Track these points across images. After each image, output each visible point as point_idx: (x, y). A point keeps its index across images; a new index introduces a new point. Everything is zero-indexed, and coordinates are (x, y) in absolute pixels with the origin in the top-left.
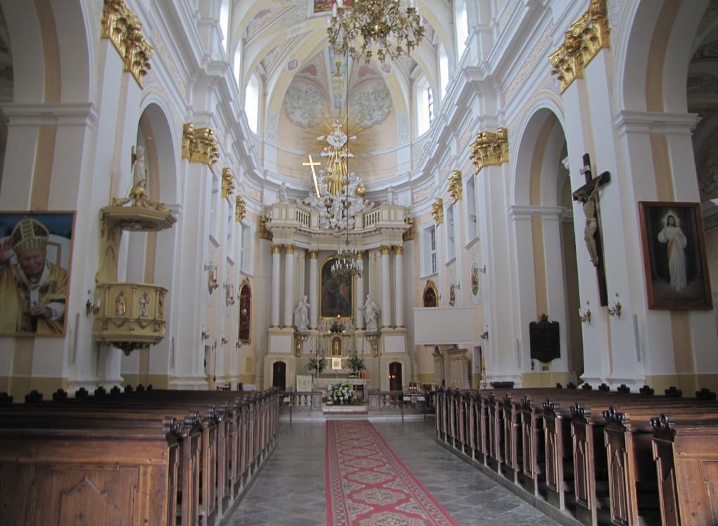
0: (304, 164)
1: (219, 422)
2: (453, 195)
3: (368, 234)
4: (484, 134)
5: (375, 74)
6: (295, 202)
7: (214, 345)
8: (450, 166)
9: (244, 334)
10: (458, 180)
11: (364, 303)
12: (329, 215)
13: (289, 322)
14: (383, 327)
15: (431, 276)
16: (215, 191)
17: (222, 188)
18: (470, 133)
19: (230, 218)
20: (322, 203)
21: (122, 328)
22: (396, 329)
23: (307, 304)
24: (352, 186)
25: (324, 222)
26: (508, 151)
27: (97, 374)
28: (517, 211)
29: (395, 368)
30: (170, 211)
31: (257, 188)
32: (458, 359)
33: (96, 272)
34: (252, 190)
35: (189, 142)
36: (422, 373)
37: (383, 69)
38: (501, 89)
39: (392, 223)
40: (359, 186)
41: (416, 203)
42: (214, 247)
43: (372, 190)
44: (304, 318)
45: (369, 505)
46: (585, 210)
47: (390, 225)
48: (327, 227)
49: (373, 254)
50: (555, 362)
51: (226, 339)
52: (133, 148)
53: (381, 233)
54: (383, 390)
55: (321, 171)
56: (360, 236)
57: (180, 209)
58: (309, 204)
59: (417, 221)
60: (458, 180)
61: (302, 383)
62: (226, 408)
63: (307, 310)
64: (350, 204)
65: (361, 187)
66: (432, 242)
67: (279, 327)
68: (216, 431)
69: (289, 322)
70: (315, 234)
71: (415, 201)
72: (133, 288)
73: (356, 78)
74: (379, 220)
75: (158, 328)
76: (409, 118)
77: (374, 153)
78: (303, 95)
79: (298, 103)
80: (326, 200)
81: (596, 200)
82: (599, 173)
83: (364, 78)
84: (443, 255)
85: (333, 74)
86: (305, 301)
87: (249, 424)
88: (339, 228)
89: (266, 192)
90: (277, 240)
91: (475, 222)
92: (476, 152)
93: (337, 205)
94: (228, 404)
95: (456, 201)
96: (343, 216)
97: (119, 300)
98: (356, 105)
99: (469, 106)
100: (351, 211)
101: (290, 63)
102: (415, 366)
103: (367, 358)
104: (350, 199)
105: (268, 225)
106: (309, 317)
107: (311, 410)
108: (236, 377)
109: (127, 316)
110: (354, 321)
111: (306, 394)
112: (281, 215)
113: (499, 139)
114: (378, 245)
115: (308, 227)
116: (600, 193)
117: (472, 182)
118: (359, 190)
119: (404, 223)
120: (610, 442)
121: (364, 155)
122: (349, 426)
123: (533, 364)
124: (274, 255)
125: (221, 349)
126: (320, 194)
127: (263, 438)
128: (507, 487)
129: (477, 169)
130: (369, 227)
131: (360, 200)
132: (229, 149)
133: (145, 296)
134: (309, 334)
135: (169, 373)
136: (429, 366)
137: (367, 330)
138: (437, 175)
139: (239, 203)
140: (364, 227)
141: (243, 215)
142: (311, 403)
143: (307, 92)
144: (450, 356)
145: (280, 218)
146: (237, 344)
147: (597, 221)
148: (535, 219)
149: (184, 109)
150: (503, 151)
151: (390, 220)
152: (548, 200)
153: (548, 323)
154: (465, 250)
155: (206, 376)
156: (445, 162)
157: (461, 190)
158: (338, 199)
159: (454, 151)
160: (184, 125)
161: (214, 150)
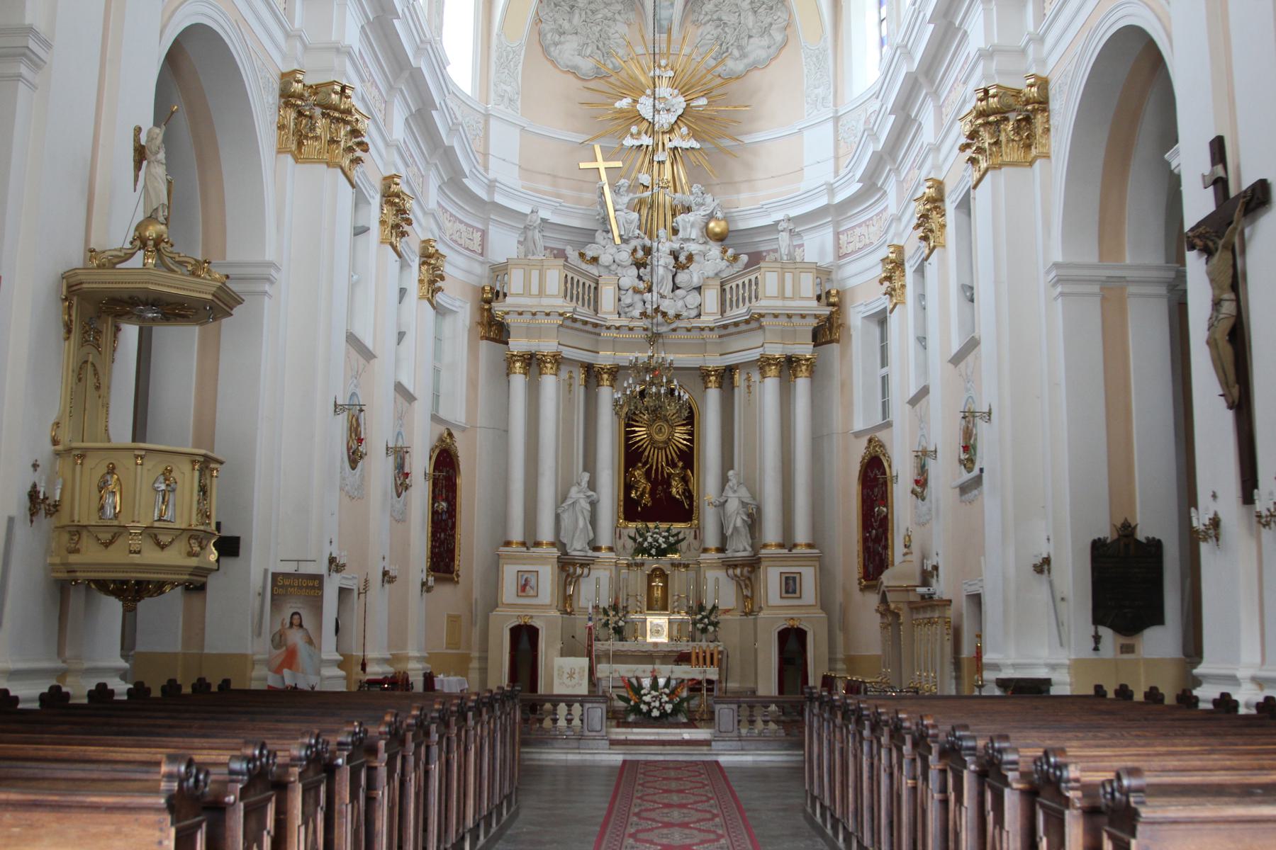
0: (582, 165)
1: (338, 766)
2: (925, 238)
3: (732, 330)
4: (991, 92)
6: (561, 254)
7: (362, 587)
9: (443, 559)
10: (936, 201)
11: (723, 489)
12: (642, 286)
13: (546, 534)
14: (765, 546)
16: (360, 231)
17: (383, 222)
18: (961, 92)
19: (403, 291)
20: (625, 256)
21: (111, 548)
22: (794, 551)
23: (591, 493)
25: (628, 301)
26: (1048, 130)
27: (60, 653)
28: (1064, 276)
29: (792, 642)
30: (227, 277)
31: (476, 224)
32: (930, 622)
33: (53, 418)
34: (462, 227)
35: (294, 115)
40: (711, 216)
41: (846, 255)
42: (362, 361)
43: (742, 225)
46: (1209, 273)
47: (784, 308)
48: (636, 313)
49: (744, 376)
51: (392, 573)
52: (138, 130)
54: (762, 691)
55: (622, 181)
56: (714, 335)
58: (595, 260)
59: (848, 299)
60: (936, 201)
61: (566, 675)
62: (355, 734)
63: (588, 507)
64: (690, 258)
65: (717, 219)
67: (524, 544)
68: (323, 788)
70: (608, 328)
72: (137, 457)
74: (757, 298)
75: (196, 549)
76: (830, 52)
77: (747, 139)
79: (570, 21)
80: (635, 250)
81: (1236, 252)
82: (1248, 181)
84: (904, 384)
87: (427, 772)
88: (664, 314)
90: (518, 345)
91: (972, 300)
92: (973, 135)
93: (662, 261)
94: (361, 724)
96: (676, 287)
97: (106, 482)
99: (961, 23)
103: (728, 617)
104: (693, 247)
105: (498, 308)
106: (593, 521)
107: (581, 738)
108: (419, 659)
109: (123, 521)
110: (698, 534)
111: (569, 700)
113: (1027, 102)
114: (755, 355)
115: (592, 312)
116: (1247, 231)
117: (965, 205)
118: (712, 225)
119: (815, 303)
120: (1047, 833)
121: (726, 143)
122: (672, 774)
124: (512, 377)
125: (379, 597)
126: (621, 236)
127: (471, 802)
129: (977, 175)
130: (736, 312)
131: (715, 250)
132: (398, 130)
133: (167, 474)
137: (729, 553)
138: (891, 188)
139: (429, 257)
142: (582, 720)
144: (915, 616)
146: (424, 584)
147: (1238, 300)
148: (1112, 296)
150: (1039, 130)
151: (784, 298)
152: (1142, 252)
155: (338, 657)
156: (909, 158)
157: (943, 226)
158: (664, 246)
159: (928, 134)
161: (355, 133)
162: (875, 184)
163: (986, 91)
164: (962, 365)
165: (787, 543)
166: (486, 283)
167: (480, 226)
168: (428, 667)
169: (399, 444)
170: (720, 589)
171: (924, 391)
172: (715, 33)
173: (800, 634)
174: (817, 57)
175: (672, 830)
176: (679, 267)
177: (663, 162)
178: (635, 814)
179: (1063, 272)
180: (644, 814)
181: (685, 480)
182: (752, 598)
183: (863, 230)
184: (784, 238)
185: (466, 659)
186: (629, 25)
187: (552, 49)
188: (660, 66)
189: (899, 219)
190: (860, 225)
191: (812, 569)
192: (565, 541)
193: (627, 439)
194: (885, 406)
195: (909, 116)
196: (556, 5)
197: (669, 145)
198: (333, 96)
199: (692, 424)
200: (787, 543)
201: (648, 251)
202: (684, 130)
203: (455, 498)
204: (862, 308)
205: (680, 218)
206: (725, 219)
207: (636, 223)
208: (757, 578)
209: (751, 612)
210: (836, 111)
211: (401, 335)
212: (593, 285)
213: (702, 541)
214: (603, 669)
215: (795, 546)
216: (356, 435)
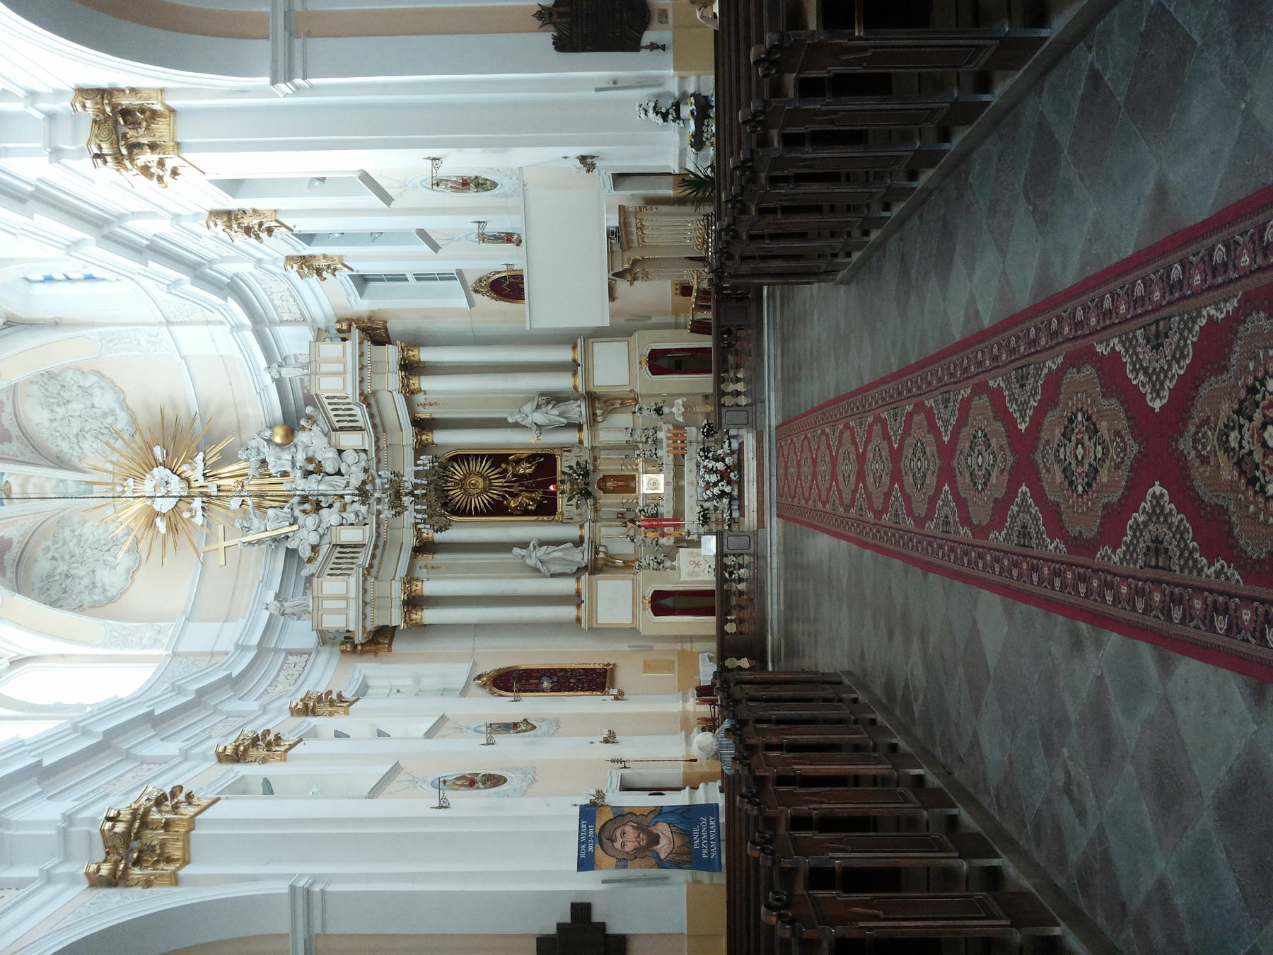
2: (270, 231)
3: (377, 420)
4: (96, 151)
6: (309, 579)
9: (594, 680)
12: (337, 505)
13: (566, 586)
14: (575, 388)
16: (268, 788)
17: (264, 760)
19: (338, 735)
20: (310, 521)
24: (269, 454)
28: (284, 71)
29: (660, 362)
32: (641, 228)
34: (283, 673)
40: (269, 441)
42: (401, 777)
43: (278, 414)
44: (559, 554)
45: (955, 433)
48: (364, 509)
49: (421, 408)
53: (374, 393)
54: (710, 390)
56: (383, 437)
57: (301, 883)
58: (315, 548)
59: (348, 313)
64: (310, 460)
66: (389, 280)
67: (578, 606)
69: (566, 586)
71: (298, 316)
76: (102, 330)
78: (62, 567)
79: (81, 578)
80: (304, 511)
83: (14, 431)
84: (416, 258)
86: (523, 552)
88: (364, 483)
89: (288, 644)
91: (323, 179)
92: (145, 170)
95: (282, 225)
96: (339, 473)
98: (81, 448)
100: (328, 459)
102: (656, 319)
104: (301, 457)
105: (359, 638)
106: (557, 543)
110: (566, 449)
117: (309, 238)
123: (653, 47)
124: (426, 621)
126: (291, 525)
128: (1054, 63)
130: (359, 417)
131: (302, 437)
132: (251, 705)
137: (583, 420)
138: (230, 269)
139: (307, 709)
140: (361, 429)
141: (334, 696)
143: (53, 558)
144: (636, 245)
145: (345, 611)
146: (616, 699)
149: (49, 891)
151: (345, 372)
154: (393, 205)
159: (244, 269)
160: (220, 761)
161: (160, 801)
162: (228, 285)
163: (97, 156)
164: (439, 243)
165: (572, 367)
169: (484, 729)
170: (616, 428)
171: (422, 234)
174: (110, 341)
175: (839, 472)
176: (319, 470)
177: (218, 487)
178: (824, 506)
179: (281, 74)
180: (807, 495)
181: (518, 462)
182: (623, 399)
183: (276, 297)
184: (287, 373)
185: (682, 653)
186: (85, 521)
187: (109, 594)
188: (124, 492)
189: (259, 260)
190: (272, 301)
194: (445, 277)
195: (148, 247)
196: (65, 592)
197: (202, 482)
199: (467, 456)
200: (572, 367)
201: (305, 499)
202: (184, 467)
204: (352, 298)
205: (272, 471)
206: (271, 427)
207: (277, 511)
210: (160, 324)
211: (381, 734)
212: (339, 549)
213: (573, 445)
215: (575, 361)
216: (470, 782)
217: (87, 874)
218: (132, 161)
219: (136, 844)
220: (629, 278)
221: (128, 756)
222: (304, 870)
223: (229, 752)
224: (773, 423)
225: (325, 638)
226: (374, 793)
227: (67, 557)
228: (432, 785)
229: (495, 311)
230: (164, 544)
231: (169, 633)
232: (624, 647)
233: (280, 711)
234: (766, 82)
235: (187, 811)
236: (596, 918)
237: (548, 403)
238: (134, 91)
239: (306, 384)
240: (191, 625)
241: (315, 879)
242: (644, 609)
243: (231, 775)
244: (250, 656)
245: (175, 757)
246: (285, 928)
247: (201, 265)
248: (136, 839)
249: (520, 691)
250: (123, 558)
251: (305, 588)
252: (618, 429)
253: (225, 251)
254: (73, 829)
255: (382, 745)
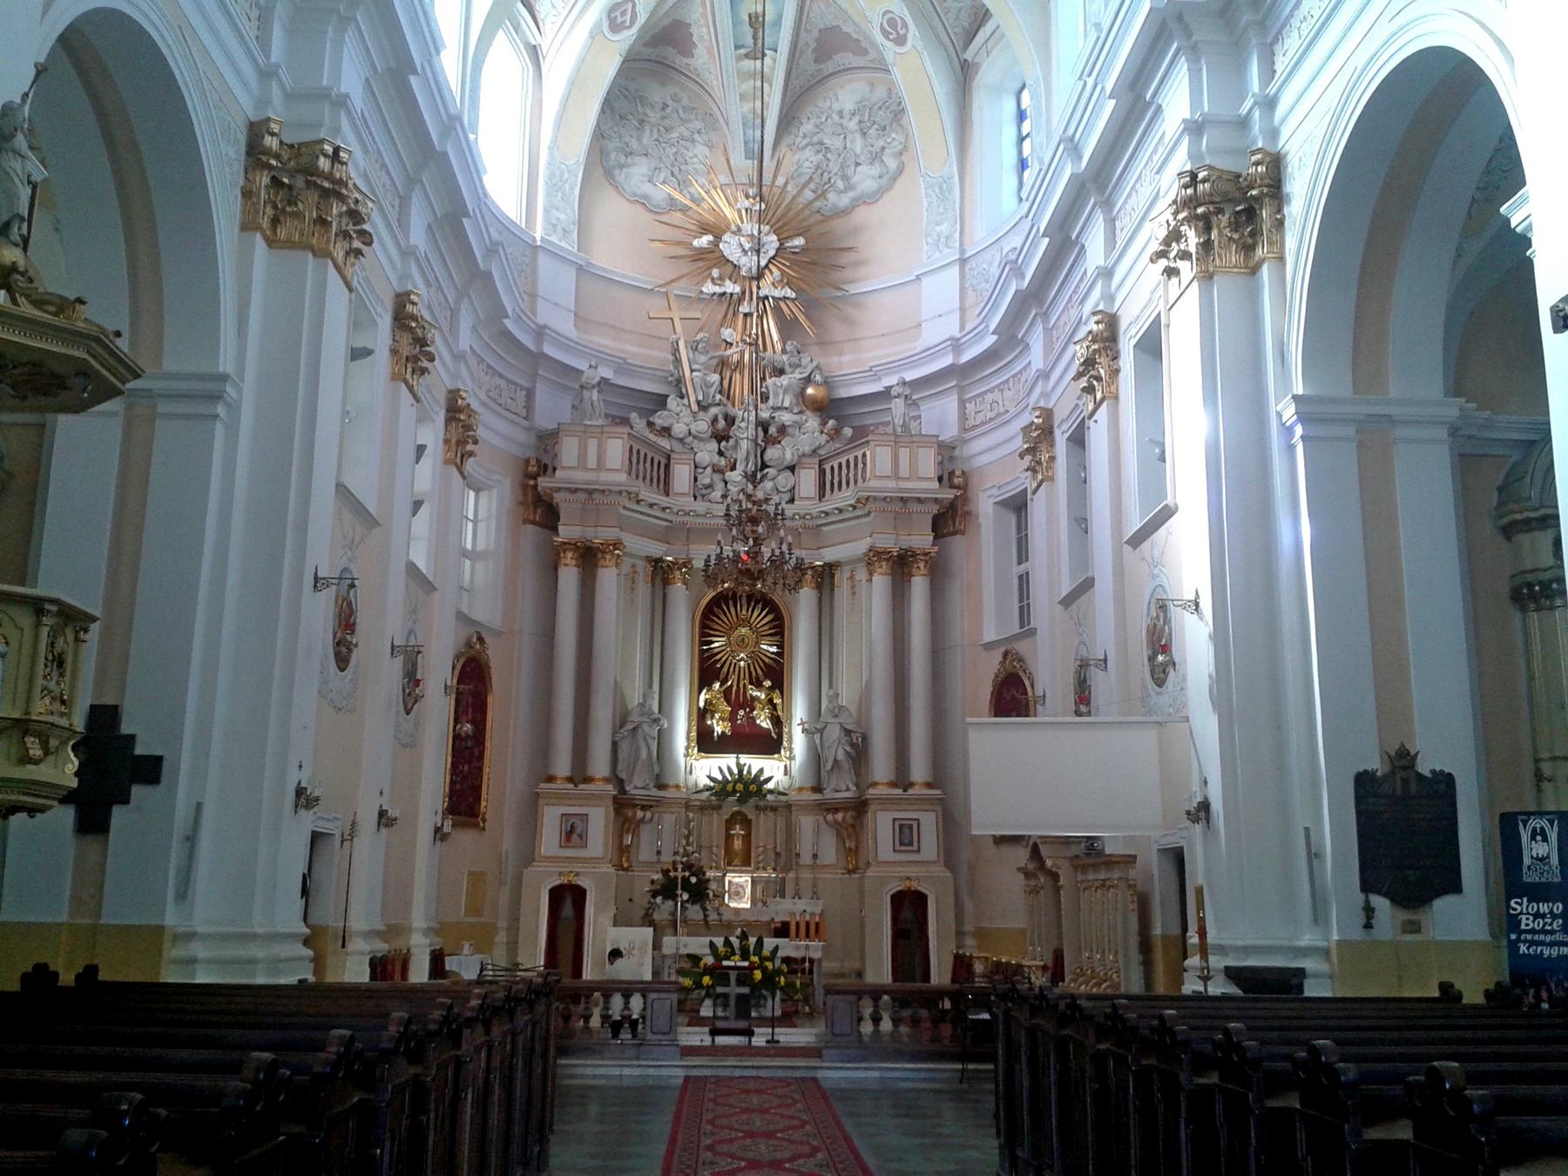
2: (1090, 390)
4: (1201, 176)
5: (865, 52)
6: (625, 421)
7: (347, 832)
8: (1082, 302)
9: (464, 801)
14: (874, 784)
15: (1015, 638)
17: (394, 352)
19: (421, 449)
20: (702, 426)
22: (910, 791)
24: (790, 379)
25: (707, 481)
29: (909, 908)
32: (1104, 885)
34: (503, 383)
36: (985, 925)
37: (885, 34)
38: (1262, 24)
39: (903, 485)
40: (808, 380)
43: (844, 393)
50: (1442, 904)
54: (871, 978)
57: (230, 390)
58: (666, 431)
66: (1019, 540)
67: (570, 780)
69: (600, 764)
71: (971, 422)
73: (807, 64)
75: (36, 751)
76: (956, 179)
77: (853, 289)
78: (654, 116)
79: (639, 139)
80: (715, 420)
83: (829, 67)
84: (1051, 572)
85: (743, 51)
92: (1175, 236)
93: (745, 433)
95: (1097, 406)
99: (1154, 96)
101: (612, 10)
102: (968, 905)
104: (786, 418)
105: (544, 483)
112: (583, 456)
117: (1079, 440)
118: (810, 391)
119: (936, 485)
123: (1369, 911)
125: (369, 848)
126: (698, 402)
131: (812, 422)
132: (465, 340)
134: (659, 802)
135: (170, 920)
136: (1008, 901)
138: (1037, 341)
139: (456, 411)
140: (822, 495)
141: (469, 447)
145: (582, 464)
146: (437, 830)
151: (897, 478)
153: (1420, 776)
154: (1127, 548)
159: (1036, 357)
160: (398, 296)
161: (355, 216)
163: (1193, 176)
164: (1074, 607)
165: (902, 780)
166: (531, 454)
167: (525, 384)
168: (438, 943)
169: (412, 642)
172: (815, 159)
173: (919, 900)
174: (941, 188)
182: (857, 851)
183: (996, 396)
184: (898, 406)
187: (617, 172)
190: (991, 390)
191: (932, 815)
192: (623, 776)
193: (702, 652)
198: (322, 159)
200: (902, 780)
201: (730, 420)
202: (776, 273)
203: (484, 720)
204: (994, 491)
208: (862, 826)
209: (854, 871)
210: (962, 251)
211: (417, 505)
214: (669, 943)
215: (911, 785)
216: (346, 621)
217: (268, 120)
218: (1187, 220)
219: (300, 182)
220: (1031, 866)
221: (412, 181)
222: (247, 396)
223: (409, 308)
224: (820, 1074)
225: (548, 440)
226: (342, 490)
227: (667, 122)
228: (345, 570)
229: (976, 679)
230: (679, 243)
231: (563, 244)
232: (508, 843)
233: (455, 376)
234: (1286, 1065)
235: (339, 252)
236: (137, 791)
237: (852, 745)
238: (1280, 224)
239: (881, 429)
240: (571, 273)
241: (234, 408)
242: (561, 874)
243: (379, 310)
244: (529, 343)
245: (407, 238)
246: (168, 365)
247: (1041, 302)
248: (308, 183)
249: (459, 693)
250: (662, 191)
251: (614, 417)
252: (816, 843)
253: (1062, 334)
254: (327, 107)
255: (402, 506)
